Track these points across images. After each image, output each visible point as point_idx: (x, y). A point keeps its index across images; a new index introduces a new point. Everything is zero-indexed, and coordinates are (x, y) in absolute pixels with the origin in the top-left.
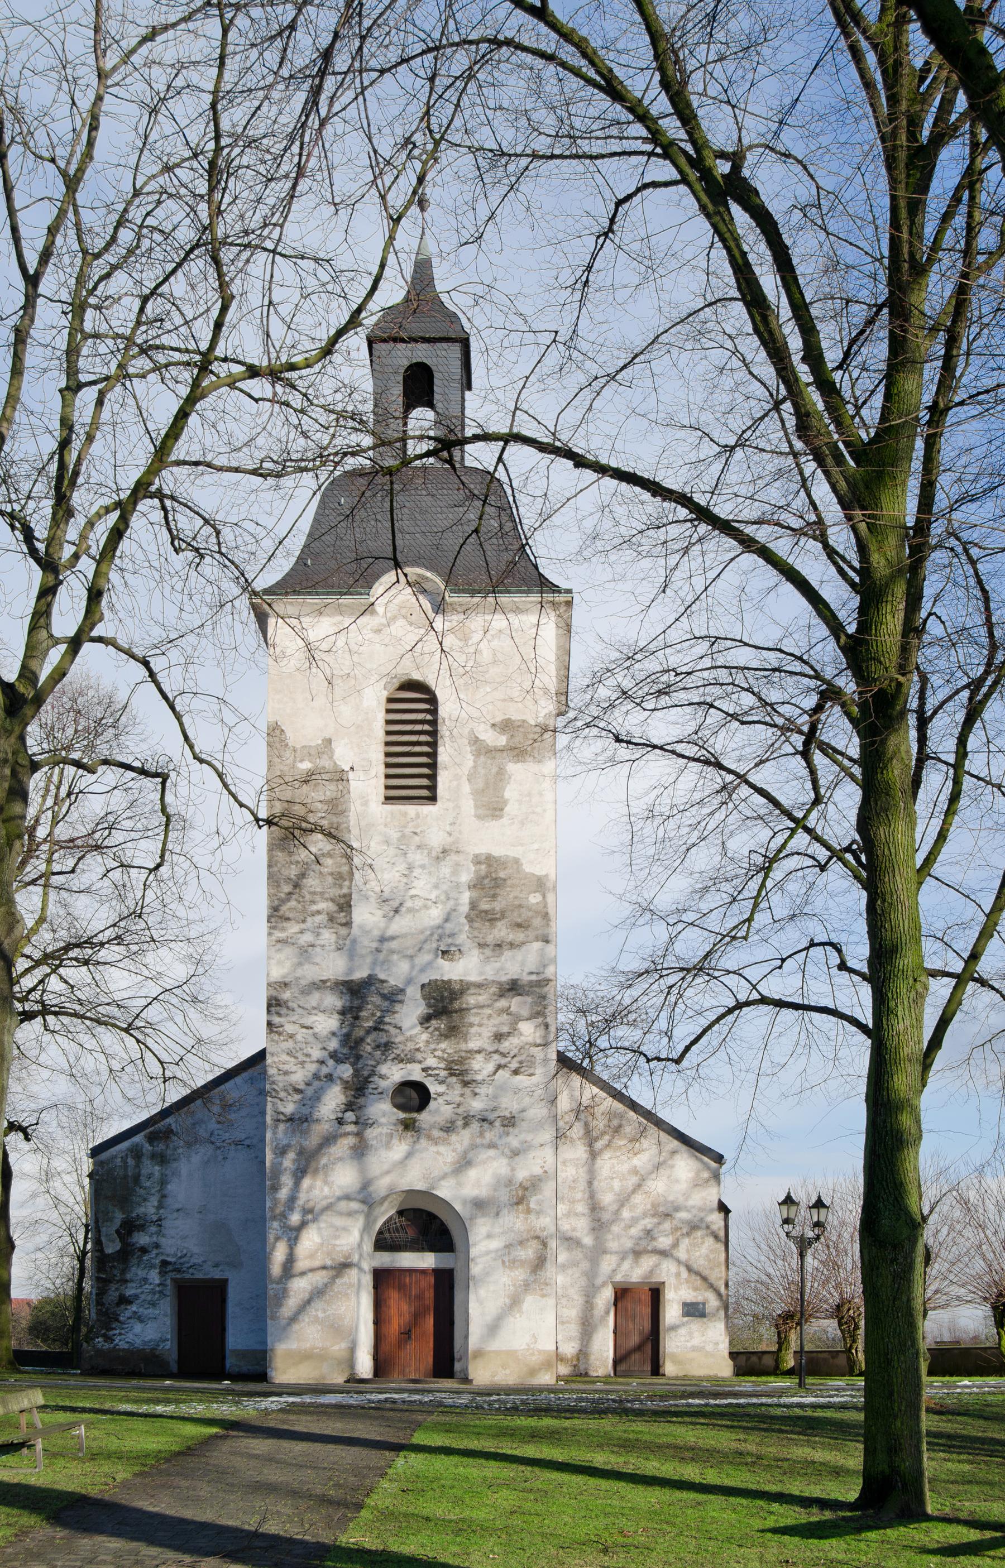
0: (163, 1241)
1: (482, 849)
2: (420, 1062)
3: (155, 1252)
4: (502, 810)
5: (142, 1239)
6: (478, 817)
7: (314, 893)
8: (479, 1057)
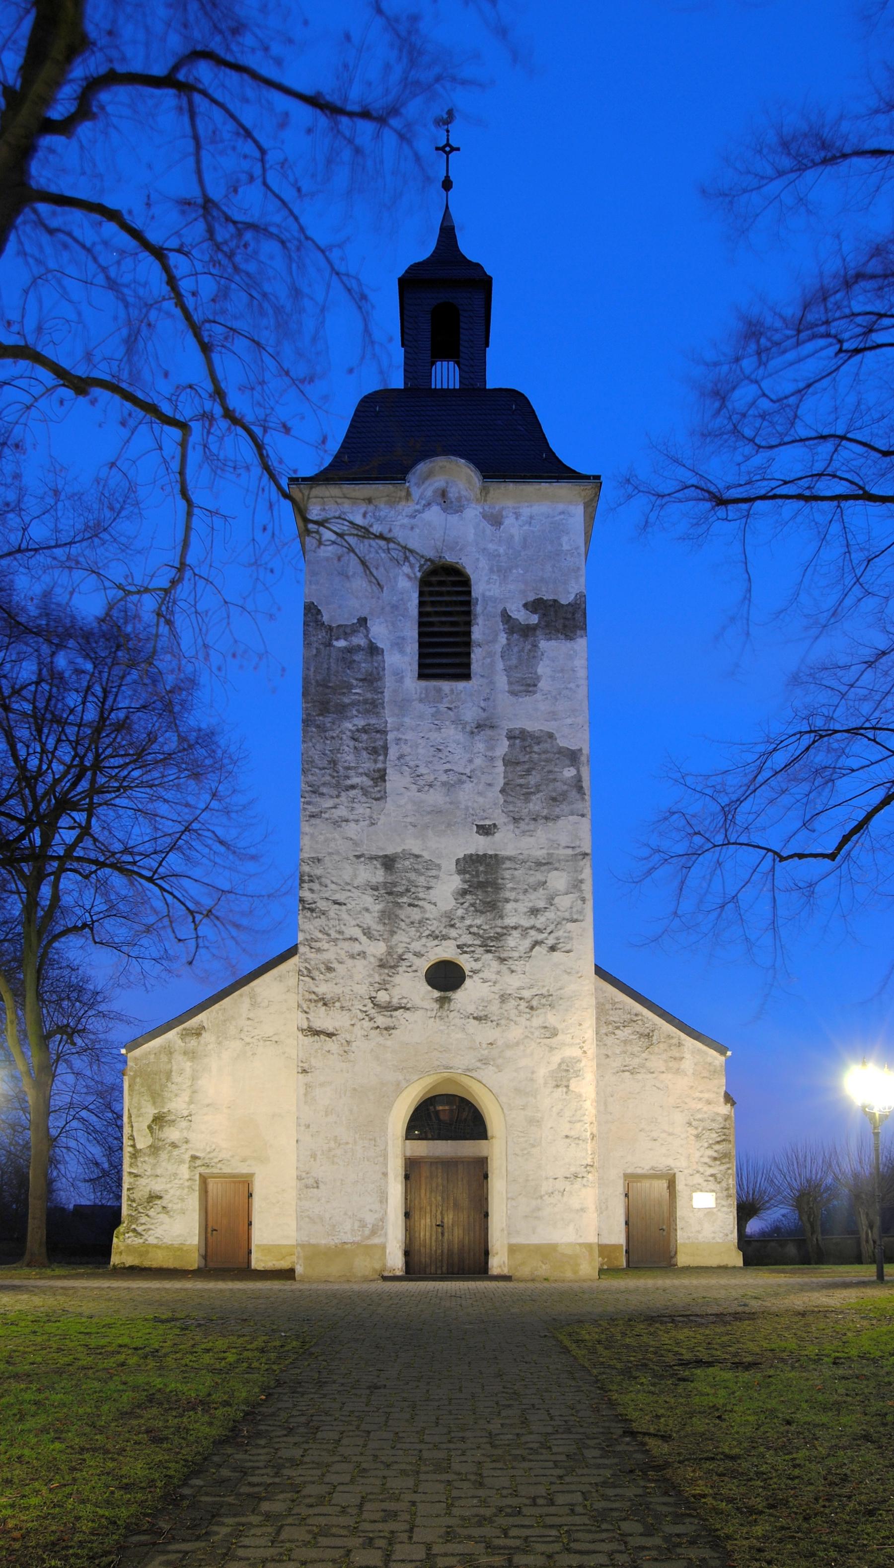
0: (192, 1136)
1: (518, 724)
2: (455, 939)
3: (185, 1146)
4: (535, 685)
5: (172, 1134)
6: (513, 693)
7: (348, 768)
8: (516, 934)
